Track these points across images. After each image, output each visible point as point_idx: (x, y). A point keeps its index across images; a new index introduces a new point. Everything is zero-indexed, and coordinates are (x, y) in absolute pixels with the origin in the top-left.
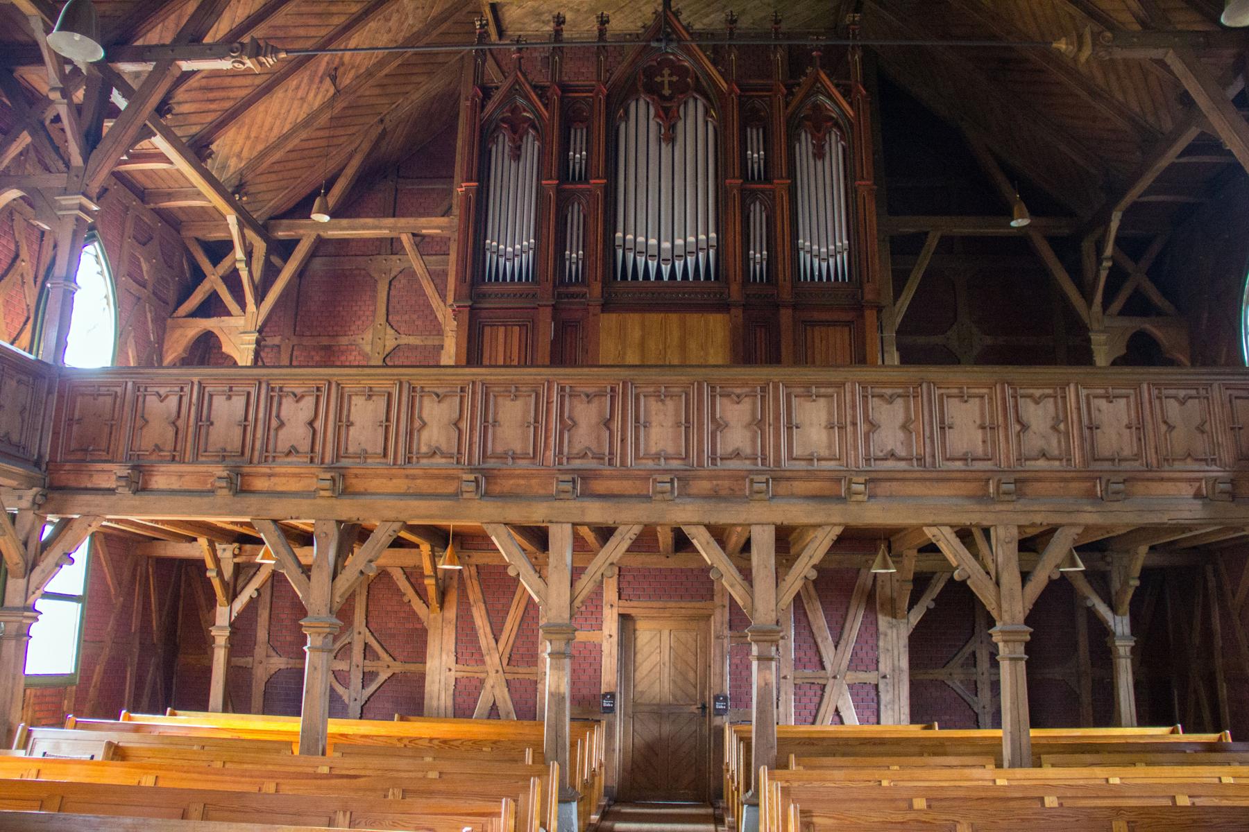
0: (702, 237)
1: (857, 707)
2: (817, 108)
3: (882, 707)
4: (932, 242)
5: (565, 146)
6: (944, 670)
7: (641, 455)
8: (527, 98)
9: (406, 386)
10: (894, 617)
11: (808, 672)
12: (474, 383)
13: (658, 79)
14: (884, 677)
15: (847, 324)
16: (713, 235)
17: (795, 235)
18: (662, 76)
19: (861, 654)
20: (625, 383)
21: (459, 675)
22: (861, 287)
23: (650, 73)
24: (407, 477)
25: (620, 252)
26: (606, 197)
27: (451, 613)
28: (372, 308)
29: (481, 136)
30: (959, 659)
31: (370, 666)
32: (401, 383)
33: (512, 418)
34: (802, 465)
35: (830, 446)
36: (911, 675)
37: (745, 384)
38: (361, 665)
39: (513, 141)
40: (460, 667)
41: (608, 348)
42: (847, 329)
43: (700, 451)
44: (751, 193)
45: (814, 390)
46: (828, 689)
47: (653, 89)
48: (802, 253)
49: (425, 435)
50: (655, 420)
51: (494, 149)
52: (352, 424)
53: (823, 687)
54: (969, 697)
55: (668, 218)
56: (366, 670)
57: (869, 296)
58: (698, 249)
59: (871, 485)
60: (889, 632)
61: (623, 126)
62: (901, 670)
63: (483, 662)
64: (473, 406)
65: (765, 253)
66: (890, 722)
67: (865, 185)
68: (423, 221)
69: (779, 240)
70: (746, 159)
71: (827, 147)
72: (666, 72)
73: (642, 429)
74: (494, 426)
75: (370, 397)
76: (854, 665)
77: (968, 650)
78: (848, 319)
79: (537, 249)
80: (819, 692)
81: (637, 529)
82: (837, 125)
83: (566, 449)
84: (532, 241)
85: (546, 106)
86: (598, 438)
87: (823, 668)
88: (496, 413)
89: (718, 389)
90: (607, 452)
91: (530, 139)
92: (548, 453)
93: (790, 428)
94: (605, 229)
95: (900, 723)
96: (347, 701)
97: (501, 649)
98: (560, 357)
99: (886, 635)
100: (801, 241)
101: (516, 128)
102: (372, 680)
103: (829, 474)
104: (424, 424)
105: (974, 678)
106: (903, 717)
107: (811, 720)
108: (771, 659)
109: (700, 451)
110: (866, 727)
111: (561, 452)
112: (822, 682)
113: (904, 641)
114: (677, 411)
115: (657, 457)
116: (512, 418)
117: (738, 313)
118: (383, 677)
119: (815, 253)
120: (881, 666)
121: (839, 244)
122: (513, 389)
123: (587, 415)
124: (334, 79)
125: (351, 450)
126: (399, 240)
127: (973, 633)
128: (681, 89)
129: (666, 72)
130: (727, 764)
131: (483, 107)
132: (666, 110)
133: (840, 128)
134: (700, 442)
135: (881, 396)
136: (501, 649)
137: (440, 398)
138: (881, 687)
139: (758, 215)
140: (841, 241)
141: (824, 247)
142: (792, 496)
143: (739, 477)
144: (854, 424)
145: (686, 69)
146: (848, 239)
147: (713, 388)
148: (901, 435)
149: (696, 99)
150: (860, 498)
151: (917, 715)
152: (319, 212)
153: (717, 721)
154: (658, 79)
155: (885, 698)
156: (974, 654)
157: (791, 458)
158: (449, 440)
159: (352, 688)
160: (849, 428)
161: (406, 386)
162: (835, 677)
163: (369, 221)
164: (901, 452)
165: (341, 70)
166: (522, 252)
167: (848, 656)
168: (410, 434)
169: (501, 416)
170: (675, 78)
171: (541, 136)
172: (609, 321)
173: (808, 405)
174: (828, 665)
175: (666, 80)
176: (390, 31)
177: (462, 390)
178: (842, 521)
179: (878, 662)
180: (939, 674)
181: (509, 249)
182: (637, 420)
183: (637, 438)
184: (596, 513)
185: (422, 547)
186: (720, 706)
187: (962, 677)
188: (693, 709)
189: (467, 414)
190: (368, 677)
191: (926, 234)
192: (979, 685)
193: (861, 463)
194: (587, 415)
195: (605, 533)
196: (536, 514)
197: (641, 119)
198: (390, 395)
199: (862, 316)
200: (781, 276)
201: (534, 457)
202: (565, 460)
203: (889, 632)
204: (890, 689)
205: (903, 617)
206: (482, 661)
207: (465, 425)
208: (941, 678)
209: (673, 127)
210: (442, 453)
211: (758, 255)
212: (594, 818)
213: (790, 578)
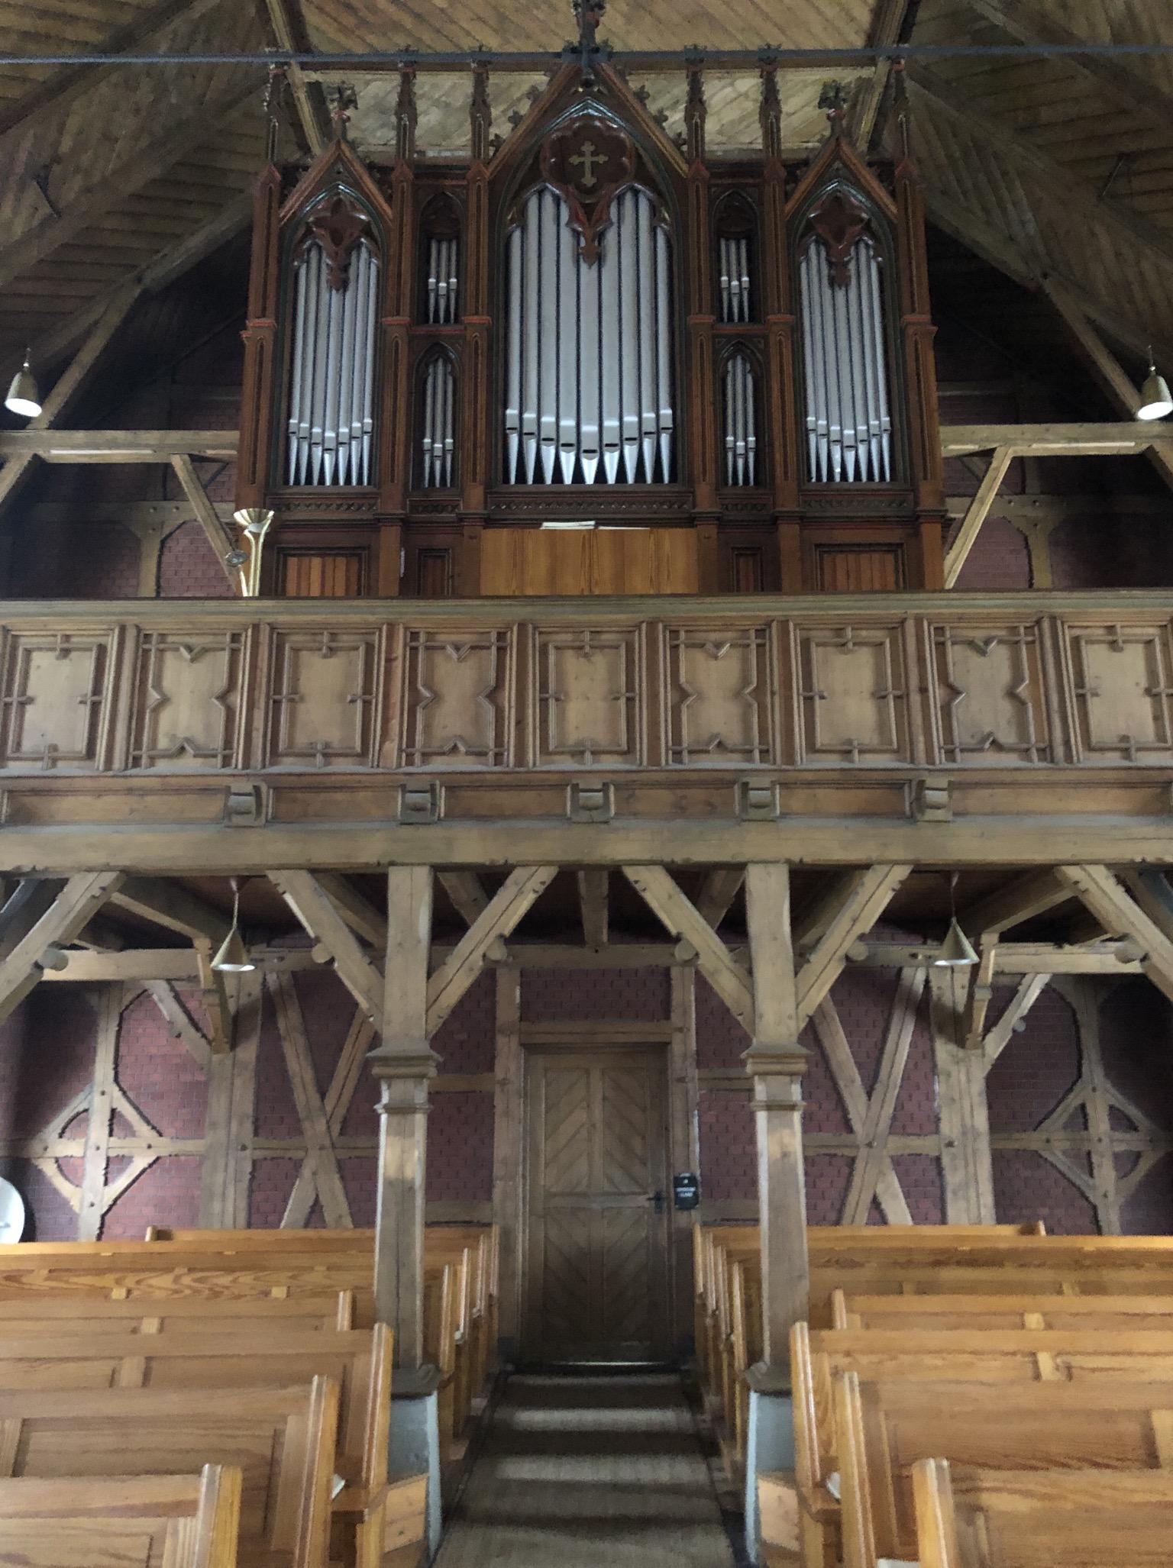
0: (648, 415)
1: (907, 1196)
2: (838, 201)
3: (949, 1196)
4: (1001, 465)
5: (422, 272)
6: (1036, 1135)
7: (551, 748)
8: (356, 184)
9: (131, 634)
10: (961, 1043)
11: (826, 1137)
12: (256, 627)
13: (575, 160)
14: (950, 1144)
15: (892, 548)
16: (666, 412)
17: (802, 412)
18: (581, 154)
19: (910, 1107)
20: (522, 626)
21: (259, 1154)
22: (915, 490)
23: (565, 146)
24: (130, 791)
25: (514, 440)
26: (490, 348)
27: (248, 1051)
28: (133, 582)
29: (281, 247)
30: (1061, 1115)
31: (118, 1145)
32: (123, 629)
33: (324, 686)
34: (833, 762)
35: (882, 726)
36: (992, 1142)
37: (727, 626)
38: (103, 1147)
39: (334, 256)
40: (261, 1141)
41: (496, 578)
42: (890, 557)
43: (654, 738)
44: (727, 346)
45: (849, 633)
46: (859, 1165)
47: (564, 175)
48: (812, 437)
49: (165, 718)
50: (575, 687)
51: (303, 271)
52: (31, 700)
53: (852, 1160)
54: (1080, 1178)
55: (590, 389)
56: (113, 1154)
57: (928, 502)
58: (642, 434)
59: (956, 794)
60: (954, 1069)
61: (517, 236)
62: (976, 1135)
63: (300, 1132)
64: (254, 667)
65: (752, 439)
66: (964, 1220)
67: (920, 319)
68: (207, 436)
69: (777, 415)
70: (720, 290)
71: (852, 266)
72: (588, 148)
73: (552, 703)
74: (292, 701)
75: (65, 653)
76: (900, 1124)
77: (1073, 1101)
78: (896, 540)
79: (376, 434)
80: (845, 1170)
81: (546, 875)
82: (867, 227)
83: (419, 738)
84: (368, 421)
85: (389, 199)
86: (477, 720)
87: (850, 1130)
88: (295, 679)
89: (682, 635)
90: (491, 744)
91: (364, 254)
92: (387, 745)
93: (809, 700)
94: (489, 404)
95: (980, 1223)
96: (76, 1209)
97: (329, 1108)
98: (413, 586)
99: (949, 1075)
100: (811, 419)
101: (343, 239)
102: (121, 1171)
103: (882, 776)
104: (165, 701)
105: (1086, 1147)
106: (983, 1212)
107: (833, 1216)
108: (793, 1107)
109: (654, 738)
110: (927, 1230)
111: (411, 742)
112: (847, 1152)
113: (978, 1086)
114: (612, 673)
115: (578, 753)
116: (324, 686)
117: (712, 530)
118: (140, 1163)
119: (834, 437)
120: (944, 1127)
121: (873, 422)
122: (325, 638)
123: (457, 679)
124: (44, 185)
125: (27, 745)
126: (168, 466)
127: (1080, 1076)
128: (611, 174)
129: (588, 148)
130: (703, 1297)
131: (282, 202)
132: (589, 210)
133: (873, 236)
134: (654, 724)
135: (971, 644)
136: (329, 1108)
137: (197, 654)
138: (946, 1161)
139: (739, 381)
140: (878, 418)
141: (847, 427)
142: (817, 813)
143: (722, 782)
144: (923, 690)
145: (620, 143)
146: (890, 413)
147: (675, 633)
148: (1006, 707)
149: (636, 193)
150: (940, 814)
151: (1009, 1205)
152: (20, 395)
153: (682, 1219)
154: (575, 160)
155: (952, 1179)
156: (1083, 1107)
157: (812, 748)
158: (208, 727)
159: (86, 1183)
160: (915, 698)
161: (131, 634)
162: (870, 1145)
163: (120, 435)
164: (1008, 737)
165: (57, 169)
166: (351, 438)
167: (889, 1110)
168: (137, 715)
169: (306, 684)
170: (602, 159)
171: (380, 250)
172: (497, 542)
173: (839, 660)
174: (857, 1126)
175: (588, 160)
176: (137, 111)
177: (235, 638)
178: (910, 857)
179: (938, 1119)
180: (1032, 1141)
181: (330, 434)
182: (544, 687)
183: (544, 721)
184: (472, 846)
185: (197, 943)
186: (688, 1192)
187: (1067, 1145)
188: (642, 1201)
189: (243, 679)
190: (113, 1165)
191: (993, 450)
192: (1095, 1159)
193: (939, 757)
194: (457, 679)
195: (491, 879)
196: (367, 849)
197: (547, 227)
198: (102, 650)
199: (917, 534)
200: (779, 471)
201: (364, 753)
202: (417, 758)
203: (954, 1069)
204: (961, 1163)
205: (975, 1047)
206: (297, 1130)
207: (240, 700)
208: (1034, 1146)
209: (601, 236)
210: (196, 748)
211: (741, 443)
212: (479, 1403)
213: (817, 959)
